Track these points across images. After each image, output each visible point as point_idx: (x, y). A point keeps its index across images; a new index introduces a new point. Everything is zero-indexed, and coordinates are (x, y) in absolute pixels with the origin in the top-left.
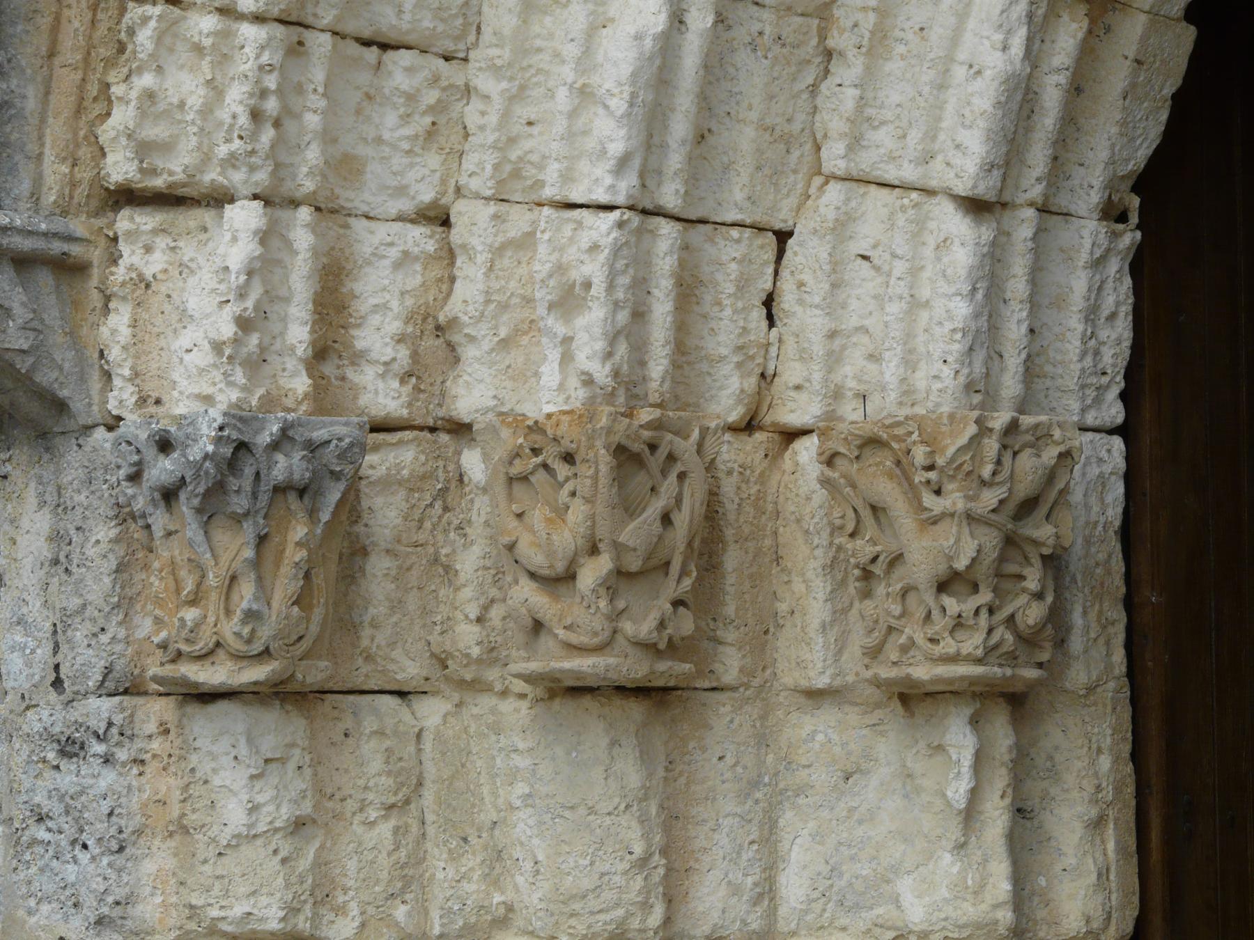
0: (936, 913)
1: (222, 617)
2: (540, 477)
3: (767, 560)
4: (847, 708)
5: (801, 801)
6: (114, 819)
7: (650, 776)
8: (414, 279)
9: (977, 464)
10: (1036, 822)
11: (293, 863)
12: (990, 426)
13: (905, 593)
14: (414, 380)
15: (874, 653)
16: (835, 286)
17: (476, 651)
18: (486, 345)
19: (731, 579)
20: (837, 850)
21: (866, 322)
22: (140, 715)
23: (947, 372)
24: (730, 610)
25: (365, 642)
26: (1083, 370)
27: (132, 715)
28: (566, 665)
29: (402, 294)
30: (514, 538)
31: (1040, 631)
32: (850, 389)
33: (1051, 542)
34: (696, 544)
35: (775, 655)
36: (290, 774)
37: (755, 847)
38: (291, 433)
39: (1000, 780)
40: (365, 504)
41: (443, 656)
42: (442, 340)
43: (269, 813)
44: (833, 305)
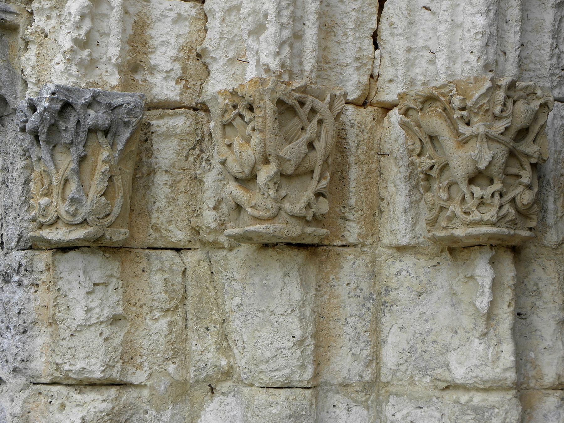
0: (470, 373)
1: (60, 202)
2: (238, 122)
3: (374, 175)
4: (419, 256)
5: (393, 308)
6: (21, 316)
7: (306, 293)
8: (185, 28)
9: (491, 106)
10: (528, 321)
11: (111, 341)
12: (499, 83)
13: (449, 187)
14: (184, 81)
15: (433, 223)
16: (410, 23)
17: (213, 225)
18: (221, 62)
19: (353, 184)
20: (414, 336)
21: (428, 43)
22: (36, 259)
23: (473, 58)
24: (353, 201)
25: (154, 221)
26: (552, 65)
27: (32, 260)
28: (252, 228)
29: (177, 36)
30: (225, 158)
31: (529, 209)
32: (420, 81)
33: (536, 155)
34: (330, 161)
35: (380, 228)
36: (110, 292)
37: (367, 334)
38: (98, 99)
39: (508, 295)
40: (155, 146)
41: (197, 229)
42: (200, 61)
43: (97, 313)
44: (409, 35)
